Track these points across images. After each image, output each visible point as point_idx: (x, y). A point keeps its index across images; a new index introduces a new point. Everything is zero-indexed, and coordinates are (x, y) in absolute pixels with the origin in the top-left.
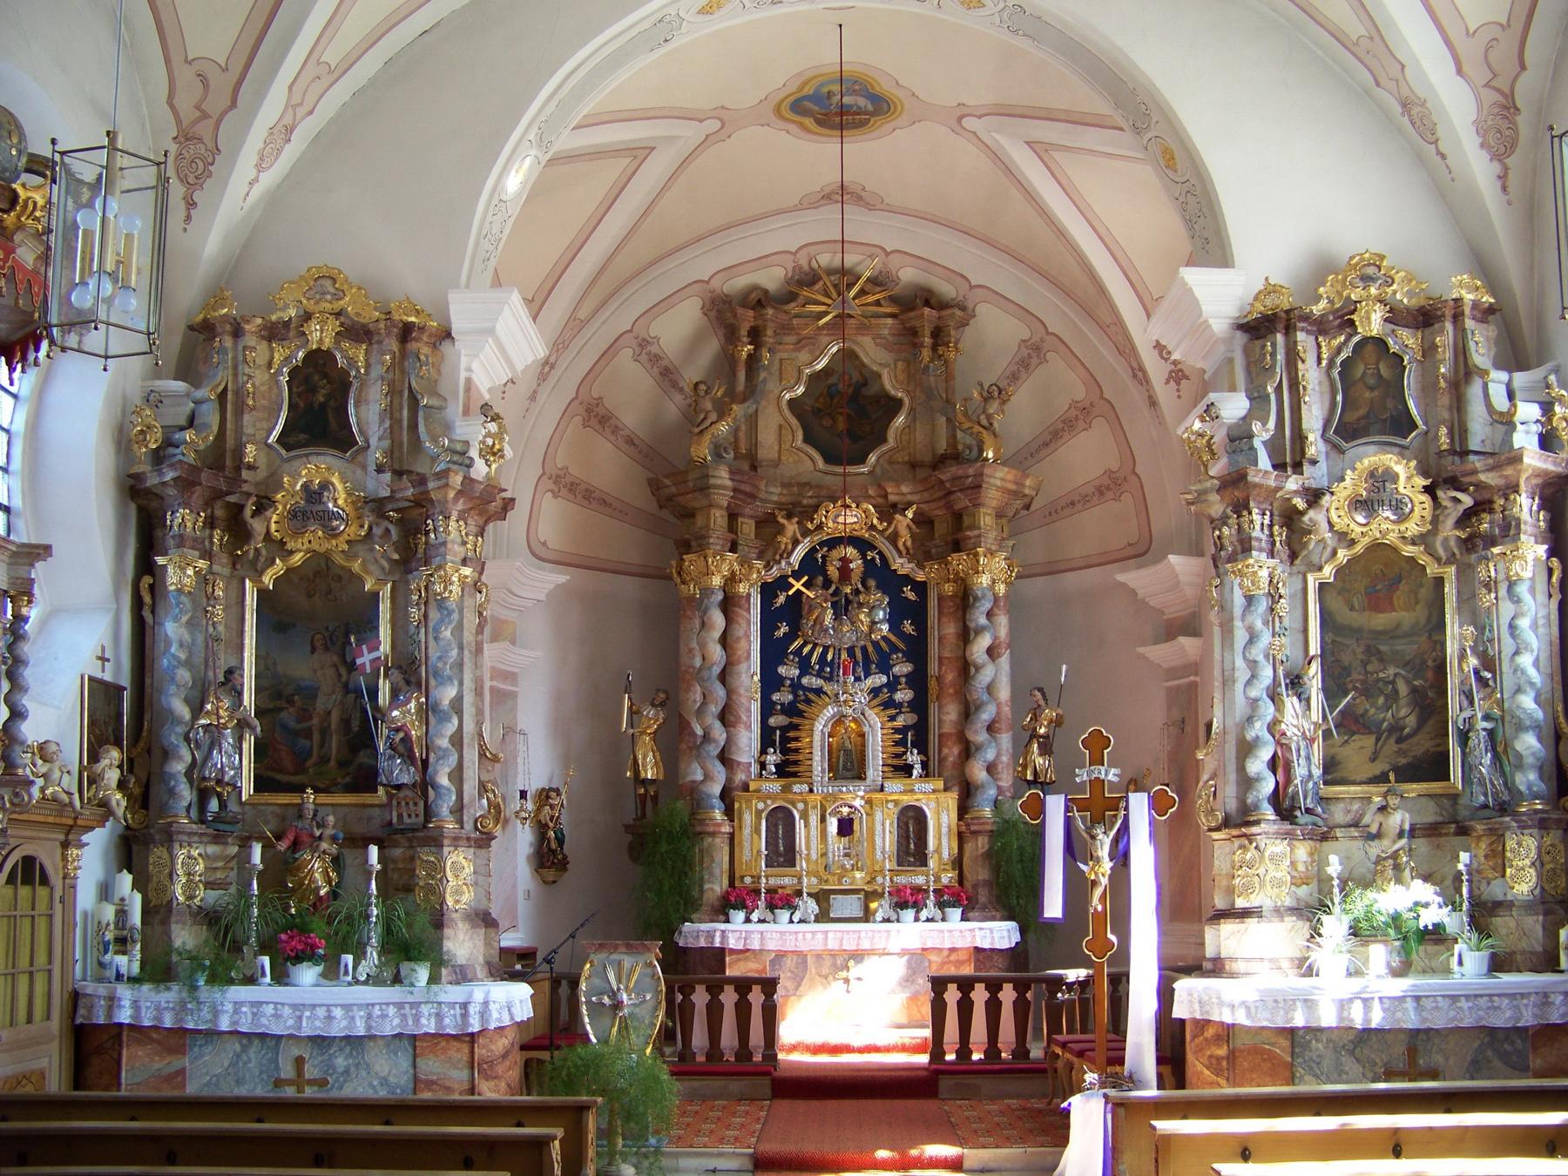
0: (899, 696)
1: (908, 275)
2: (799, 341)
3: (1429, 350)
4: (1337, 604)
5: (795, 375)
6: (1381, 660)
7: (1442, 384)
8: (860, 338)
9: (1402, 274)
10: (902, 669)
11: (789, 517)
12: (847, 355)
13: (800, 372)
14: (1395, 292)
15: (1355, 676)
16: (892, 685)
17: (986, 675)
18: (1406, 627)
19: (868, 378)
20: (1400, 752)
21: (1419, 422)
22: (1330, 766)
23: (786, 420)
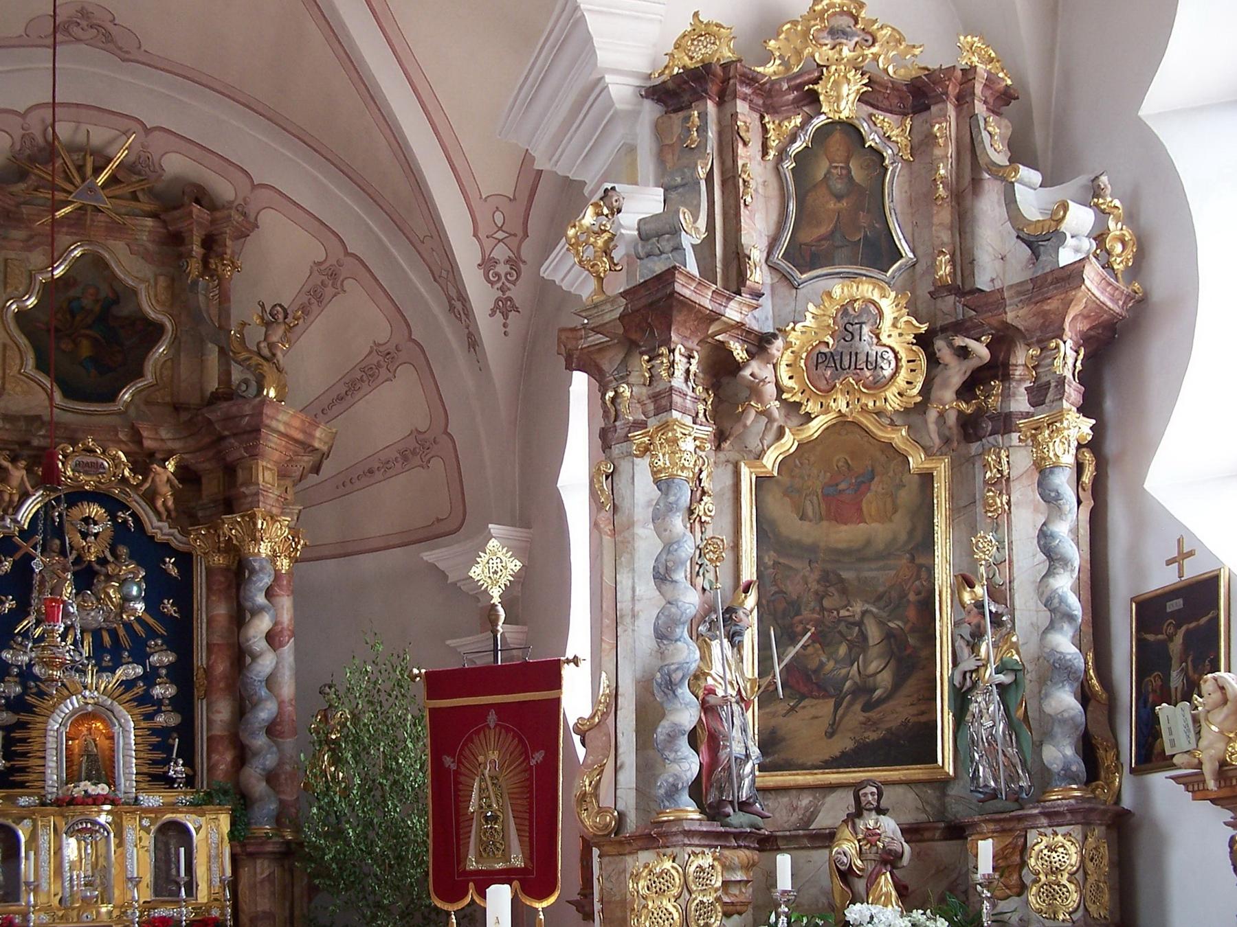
0: (158, 691)
1: (175, 165)
2: (31, 237)
3: (923, 145)
4: (780, 509)
5: (26, 281)
6: (844, 592)
7: (941, 191)
8: (111, 242)
9: (887, 32)
10: (162, 658)
11: (14, 460)
12: (96, 262)
13: (31, 277)
14: (876, 58)
15: (806, 614)
16: (150, 678)
17: (266, 663)
18: (880, 545)
19: (119, 294)
20: (869, 724)
21: (904, 247)
22: (768, 742)
23: (11, 338)
